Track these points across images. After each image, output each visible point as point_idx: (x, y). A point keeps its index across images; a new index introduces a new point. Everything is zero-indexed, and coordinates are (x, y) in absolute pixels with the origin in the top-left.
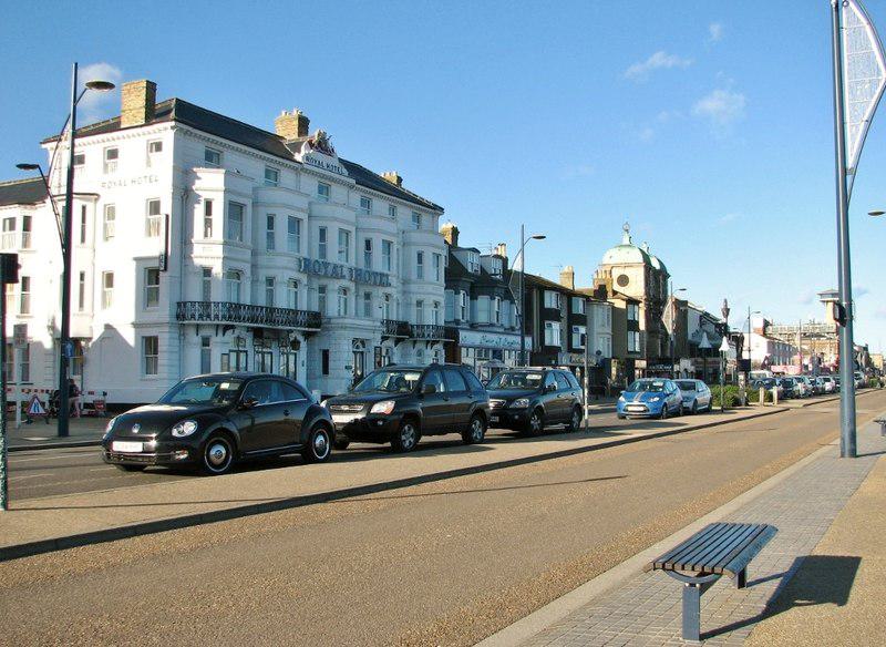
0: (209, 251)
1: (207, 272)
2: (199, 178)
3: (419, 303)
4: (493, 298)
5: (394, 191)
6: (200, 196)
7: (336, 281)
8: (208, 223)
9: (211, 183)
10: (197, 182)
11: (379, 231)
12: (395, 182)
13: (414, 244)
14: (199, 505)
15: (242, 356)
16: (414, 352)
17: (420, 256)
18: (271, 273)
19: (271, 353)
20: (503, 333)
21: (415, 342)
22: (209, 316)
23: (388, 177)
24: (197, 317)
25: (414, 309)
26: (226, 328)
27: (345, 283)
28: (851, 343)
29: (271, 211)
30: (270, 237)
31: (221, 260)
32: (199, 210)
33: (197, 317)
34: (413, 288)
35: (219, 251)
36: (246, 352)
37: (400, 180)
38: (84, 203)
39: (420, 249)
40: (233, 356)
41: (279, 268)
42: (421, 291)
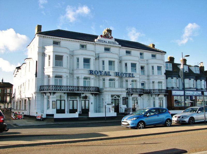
0: (49, 70)
1: (49, 76)
2: (46, 49)
3: (153, 82)
4: (201, 80)
5: (152, 49)
6: (47, 54)
7: (130, 78)
8: (49, 62)
9: (50, 50)
10: (46, 50)
11: (106, 57)
12: (152, 46)
13: (151, 64)
14: (120, 144)
15: (63, 102)
16: (152, 98)
17: (153, 67)
18: (78, 76)
19: (77, 100)
20: (195, 91)
21: (151, 95)
22: (79, 90)
23: (149, 45)
24: (45, 90)
25: (151, 85)
26: (54, 93)
27: (112, 77)
28: (43, 73)
29: (78, 57)
30: (78, 64)
31: (52, 73)
32: (47, 59)
33: (45, 90)
34: (151, 77)
35: (51, 70)
36: (65, 100)
37: (154, 45)
38: (29, 61)
39: (152, 65)
40: (59, 102)
41: (80, 74)
42: (153, 78)
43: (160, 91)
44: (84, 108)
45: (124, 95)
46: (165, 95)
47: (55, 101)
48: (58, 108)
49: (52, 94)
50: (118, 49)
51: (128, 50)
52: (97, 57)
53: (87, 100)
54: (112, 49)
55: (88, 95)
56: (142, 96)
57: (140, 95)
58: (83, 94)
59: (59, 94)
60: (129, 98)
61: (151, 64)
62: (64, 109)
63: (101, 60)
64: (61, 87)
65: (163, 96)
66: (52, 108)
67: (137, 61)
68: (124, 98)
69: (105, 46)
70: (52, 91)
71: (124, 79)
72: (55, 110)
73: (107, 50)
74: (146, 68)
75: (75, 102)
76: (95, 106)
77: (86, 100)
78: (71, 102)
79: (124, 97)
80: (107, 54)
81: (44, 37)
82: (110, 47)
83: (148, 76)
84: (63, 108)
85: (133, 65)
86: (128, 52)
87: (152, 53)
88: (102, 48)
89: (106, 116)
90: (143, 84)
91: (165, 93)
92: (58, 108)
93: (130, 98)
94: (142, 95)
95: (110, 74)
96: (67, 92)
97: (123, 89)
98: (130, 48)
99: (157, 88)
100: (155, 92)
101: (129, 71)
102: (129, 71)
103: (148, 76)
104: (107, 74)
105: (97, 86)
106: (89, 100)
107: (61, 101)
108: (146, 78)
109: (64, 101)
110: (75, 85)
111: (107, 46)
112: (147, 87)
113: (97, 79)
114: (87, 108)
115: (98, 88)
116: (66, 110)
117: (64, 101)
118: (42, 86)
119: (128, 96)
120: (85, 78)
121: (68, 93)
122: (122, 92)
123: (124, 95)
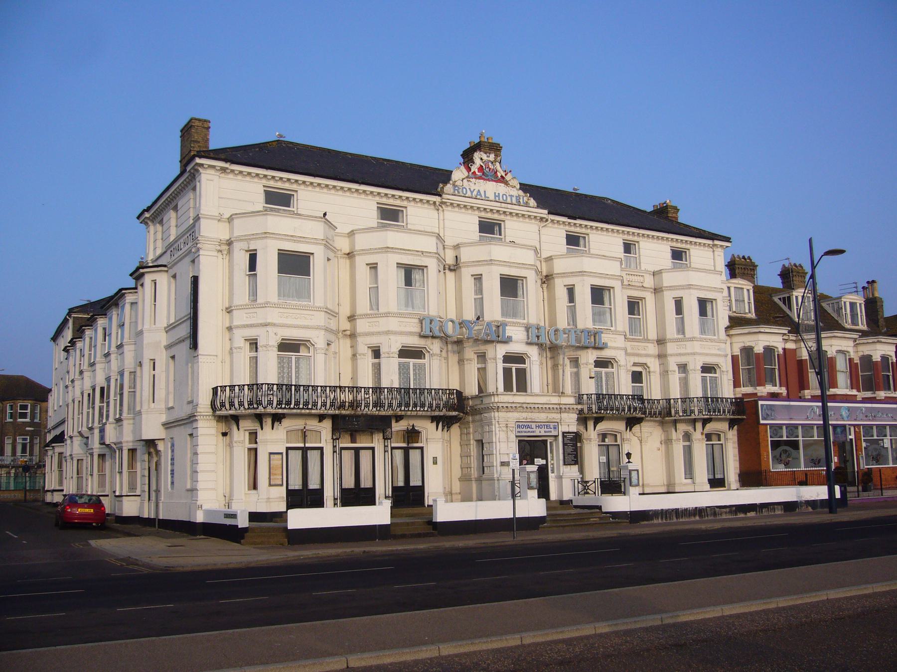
15: (313, 457)
17: (571, 291)
19: (373, 449)
24: (237, 405)
25: (366, 362)
26: (277, 418)
34: (671, 348)
43: (711, 402)
44: (401, 483)
45: (569, 423)
46: (732, 423)
47: (282, 453)
48: (296, 484)
49: (268, 421)
50: (532, 227)
51: (279, 184)
52: (450, 261)
53: (416, 445)
54: (513, 228)
55: (419, 425)
56: (636, 428)
57: (631, 422)
58: (397, 421)
59: (298, 424)
60: (585, 435)
61: (671, 288)
62: (420, 484)
63: (467, 273)
64: (391, 391)
65: (724, 426)
66: (270, 485)
67: (315, 241)
68: (571, 436)
69: (483, 214)
70: (270, 410)
71: (564, 361)
72: (282, 492)
73: (488, 228)
74: (649, 304)
75: (365, 457)
76: (710, 461)
77: (411, 445)
78: (348, 456)
79: (569, 433)
80: (393, 237)
81: (224, 170)
82: (502, 217)
83: (661, 342)
84: (366, 483)
85: (598, 295)
86: (390, 215)
87: (674, 244)
88: (469, 223)
89: (517, 516)
90: (637, 377)
91: (733, 414)
92: (349, 483)
93: (592, 435)
94: (639, 421)
95: (510, 331)
96: (331, 412)
97: (565, 400)
98: (398, 193)
99: (273, 379)
100: (315, 404)
101: (586, 318)
102: (586, 318)
103: (661, 342)
104: (497, 336)
105: (455, 385)
106: (422, 448)
107: (305, 451)
108: (653, 349)
109: (420, 450)
110: (366, 380)
111: (489, 215)
112: (654, 390)
113: (454, 359)
114: (415, 481)
115: (459, 394)
116: (329, 493)
117: (371, 451)
118: (223, 388)
119: (582, 429)
120: (405, 353)
121: (334, 418)
122: (560, 411)
123: (569, 423)
